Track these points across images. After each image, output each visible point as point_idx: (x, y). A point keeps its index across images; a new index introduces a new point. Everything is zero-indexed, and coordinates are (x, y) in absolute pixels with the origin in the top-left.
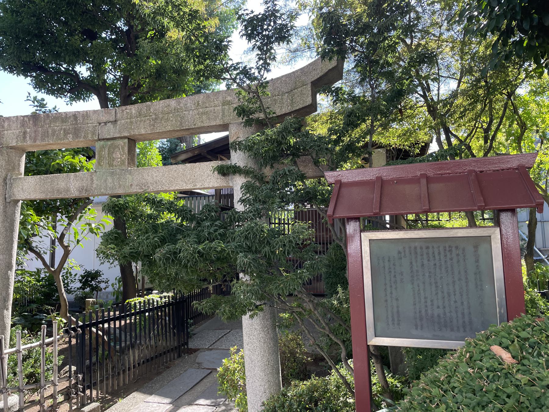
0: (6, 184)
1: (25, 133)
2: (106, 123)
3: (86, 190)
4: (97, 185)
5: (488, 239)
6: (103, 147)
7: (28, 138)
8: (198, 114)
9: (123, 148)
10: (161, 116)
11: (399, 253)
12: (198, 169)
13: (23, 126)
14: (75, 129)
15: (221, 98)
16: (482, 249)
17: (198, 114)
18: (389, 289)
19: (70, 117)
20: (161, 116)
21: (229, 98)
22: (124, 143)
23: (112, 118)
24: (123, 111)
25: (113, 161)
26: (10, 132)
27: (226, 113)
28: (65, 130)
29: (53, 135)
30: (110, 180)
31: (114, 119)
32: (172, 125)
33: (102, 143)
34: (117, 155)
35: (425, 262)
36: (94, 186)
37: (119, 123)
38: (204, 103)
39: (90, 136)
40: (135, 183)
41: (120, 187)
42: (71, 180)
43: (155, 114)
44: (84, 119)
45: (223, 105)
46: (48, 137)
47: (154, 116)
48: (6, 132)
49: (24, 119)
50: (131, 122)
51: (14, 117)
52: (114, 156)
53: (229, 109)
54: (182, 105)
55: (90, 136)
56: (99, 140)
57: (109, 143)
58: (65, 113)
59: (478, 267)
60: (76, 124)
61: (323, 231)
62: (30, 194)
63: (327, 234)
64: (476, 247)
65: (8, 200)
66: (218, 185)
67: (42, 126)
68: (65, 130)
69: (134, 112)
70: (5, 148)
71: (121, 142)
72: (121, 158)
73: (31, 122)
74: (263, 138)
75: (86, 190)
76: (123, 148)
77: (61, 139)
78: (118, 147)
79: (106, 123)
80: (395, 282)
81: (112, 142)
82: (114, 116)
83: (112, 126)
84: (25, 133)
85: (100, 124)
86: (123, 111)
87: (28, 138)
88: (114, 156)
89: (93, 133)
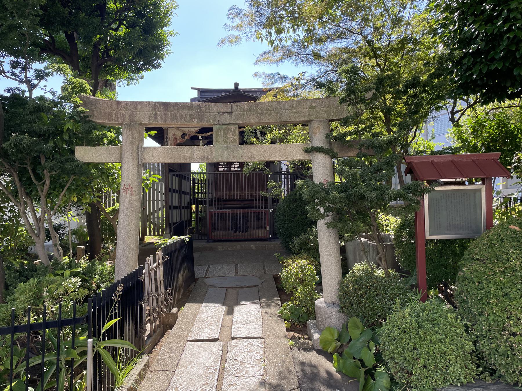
0: (139, 151)
1: (156, 115)
2: (223, 113)
3: (207, 158)
4: (216, 155)
5: (480, 190)
6: (219, 130)
7: (159, 119)
8: (292, 113)
9: (235, 131)
10: (265, 112)
11: (441, 197)
12: (289, 148)
13: (155, 109)
14: (199, 115)
15: (308, 104)
16: (478, 194)
17: (292, 113)
18: (436, 214)
19: (195, 106)
20: (265, 112)
21: (314, 105)
22: (236, 128)
23: (229, 110)
24: (237, 106)
25: (227, 139)
26: (142, 112)
27: (311, 114)
28: (190, 115)
29: (181, 119)
30: (226, 152)
31: (230, 111)
32: (273, 119)
33: (218, 126)
34: (230, 135)
35: (453, 201)
36: (214, 155)
37: (233, 114)
38: (296, 106)
39: (211, 121)
40: (245, 155)
41: (234, 157)
42: (195, 151)
43: (262, 110)
44: (206, 109)
45: (310, 108)
46: (176, 119)
47: (260, 112)
48: (138, 113)
49: (155, 104)
50: (243, 114)
51: (146, 102)
52: (228, 136)
53: (313, 111)
54: (281, 106)
55: (211, 121)
56: (218, 124)
57: (224, 127)
58: (125, 102)
59: (475, 202)
60: (201, 112)
61: (229, 190)
62: (159, 159)
63: (242, 193)
64: (475, 194)
65: (140, 163)
66: (303, 158)
67: (171, 111)
68: (190, 115)
69: (245, 107)
70: (137, 125)
71: (233, 127)
72: (233, 138)
73: (162, 107)
74: (65, 130)
75: (207, 158)
76: (235, 131)
77: (188, 122)
78: (231, 130)
79: (223, 113)
80: (439, 210)
81: (226, 126)
82: (230, 109)
83: (228, 116)
84: (156, 115)
85: (219, 113)
86: (237, 106)
87: (159, 119)
88: (228, 136)
89: (214, 120)
